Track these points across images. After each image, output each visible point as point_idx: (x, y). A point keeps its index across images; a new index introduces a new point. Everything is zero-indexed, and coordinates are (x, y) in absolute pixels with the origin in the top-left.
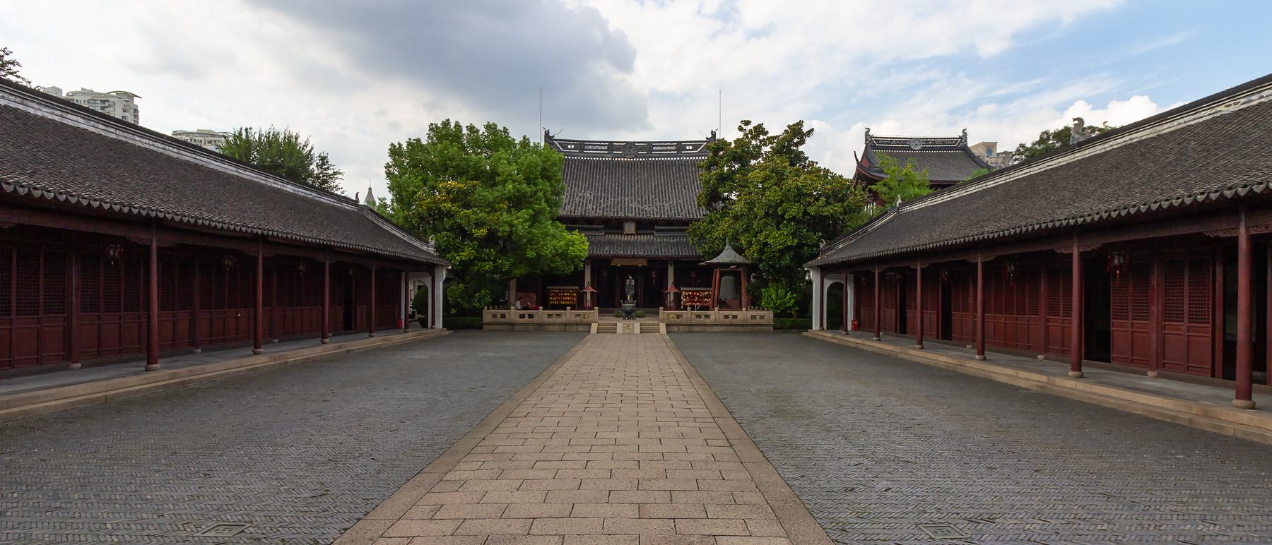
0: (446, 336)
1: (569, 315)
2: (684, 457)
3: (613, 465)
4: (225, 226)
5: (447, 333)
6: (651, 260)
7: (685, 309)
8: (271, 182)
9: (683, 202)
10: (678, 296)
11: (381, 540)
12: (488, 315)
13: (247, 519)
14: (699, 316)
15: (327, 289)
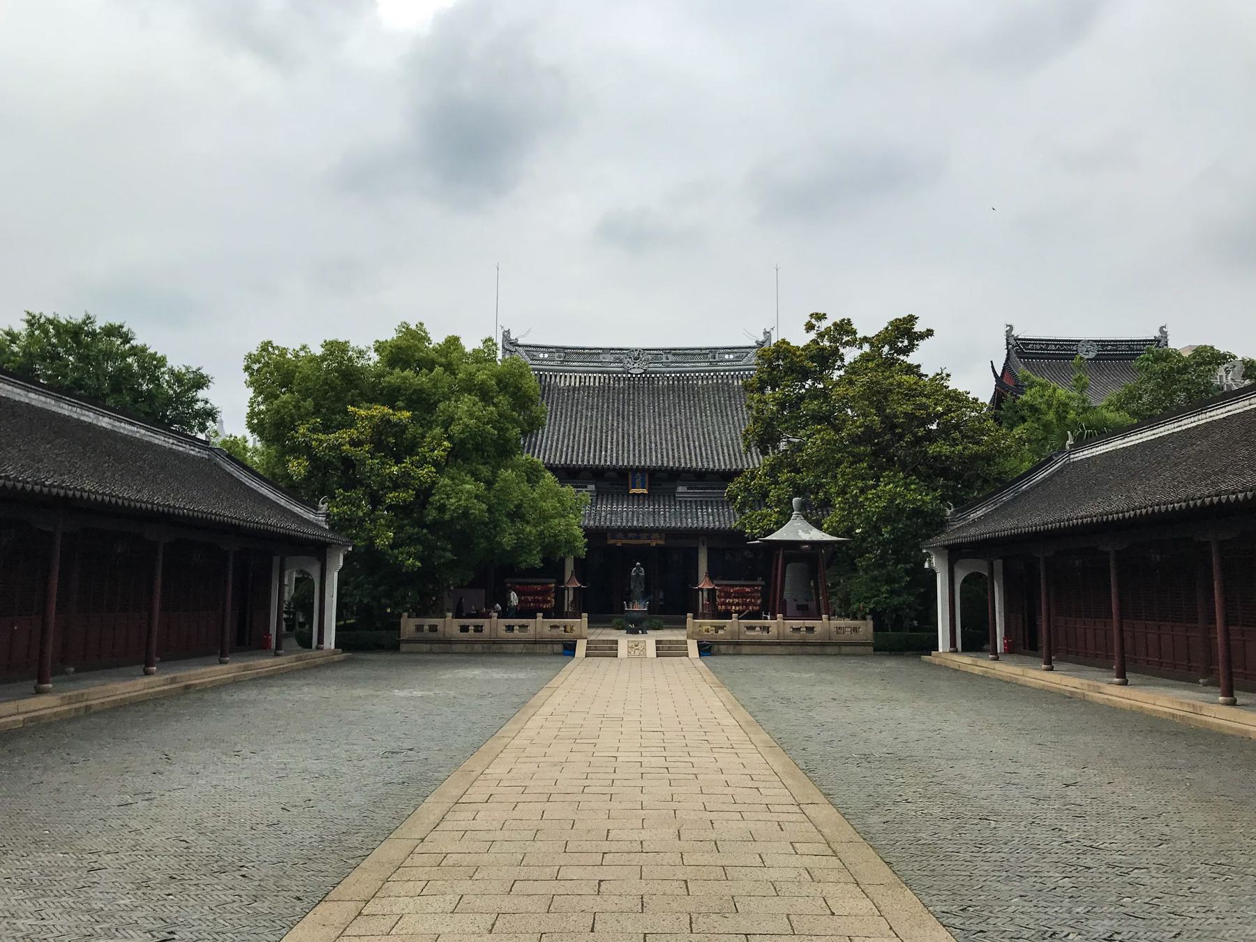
0: (340, 662)
1: (539, 626)
2: (758, 873)
3: (644, 888)
6: (671, 533)
7: (727, 615)
8: (65, 409)
9: (720, 442)
12: (408, 625)
14: (752, 628)
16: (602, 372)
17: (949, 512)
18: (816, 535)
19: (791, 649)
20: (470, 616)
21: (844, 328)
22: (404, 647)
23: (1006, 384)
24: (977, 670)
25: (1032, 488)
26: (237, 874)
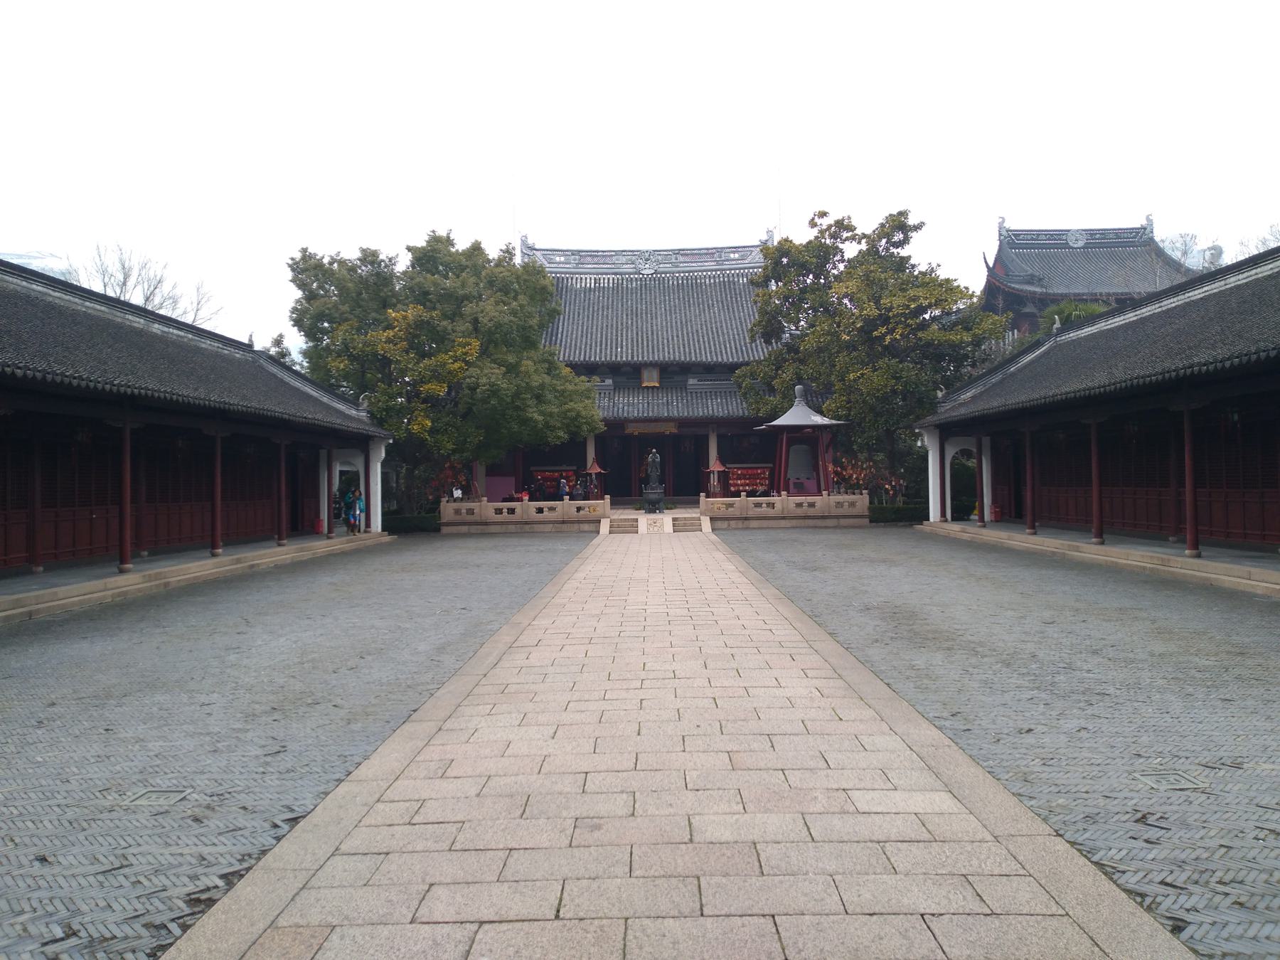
0: (389, 544)
1: (566, 507)
2: (778, 692)
4: (83, 384)
5: (387, 538)
6: (683, 423)
7: (737, 494)
10: (724, 477)
11: (380, 806)
12: (447, 510)
13: (185, 783)
14: (758, 505)
15: (219, 480)
16: (616, 274)
17: (940, 394)
18: (818, 420)
19: (794, 522)
20: (505, 500)
21: (842, 226)
22: (445, 530)
23: (997, 273)
24: (966, 536)
25: (1020, 370)
26: (330, 705)
